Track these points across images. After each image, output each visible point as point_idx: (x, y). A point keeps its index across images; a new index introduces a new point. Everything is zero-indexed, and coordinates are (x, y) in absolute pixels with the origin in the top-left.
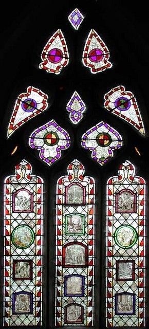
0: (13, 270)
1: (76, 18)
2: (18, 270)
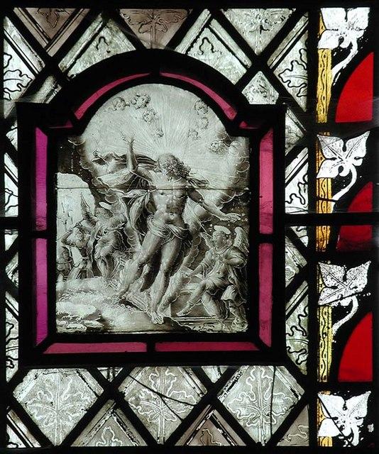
1: (345, 446)
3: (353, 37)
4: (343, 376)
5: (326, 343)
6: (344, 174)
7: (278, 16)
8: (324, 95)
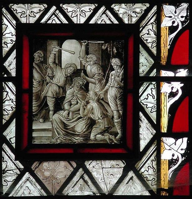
0: (19, 95)
2: (50, 91)
3: (178, 21)
4: (175, 130)
5: (165, 180)
6: (175, 25)
7: (140, 8)
8: (165, 51)
